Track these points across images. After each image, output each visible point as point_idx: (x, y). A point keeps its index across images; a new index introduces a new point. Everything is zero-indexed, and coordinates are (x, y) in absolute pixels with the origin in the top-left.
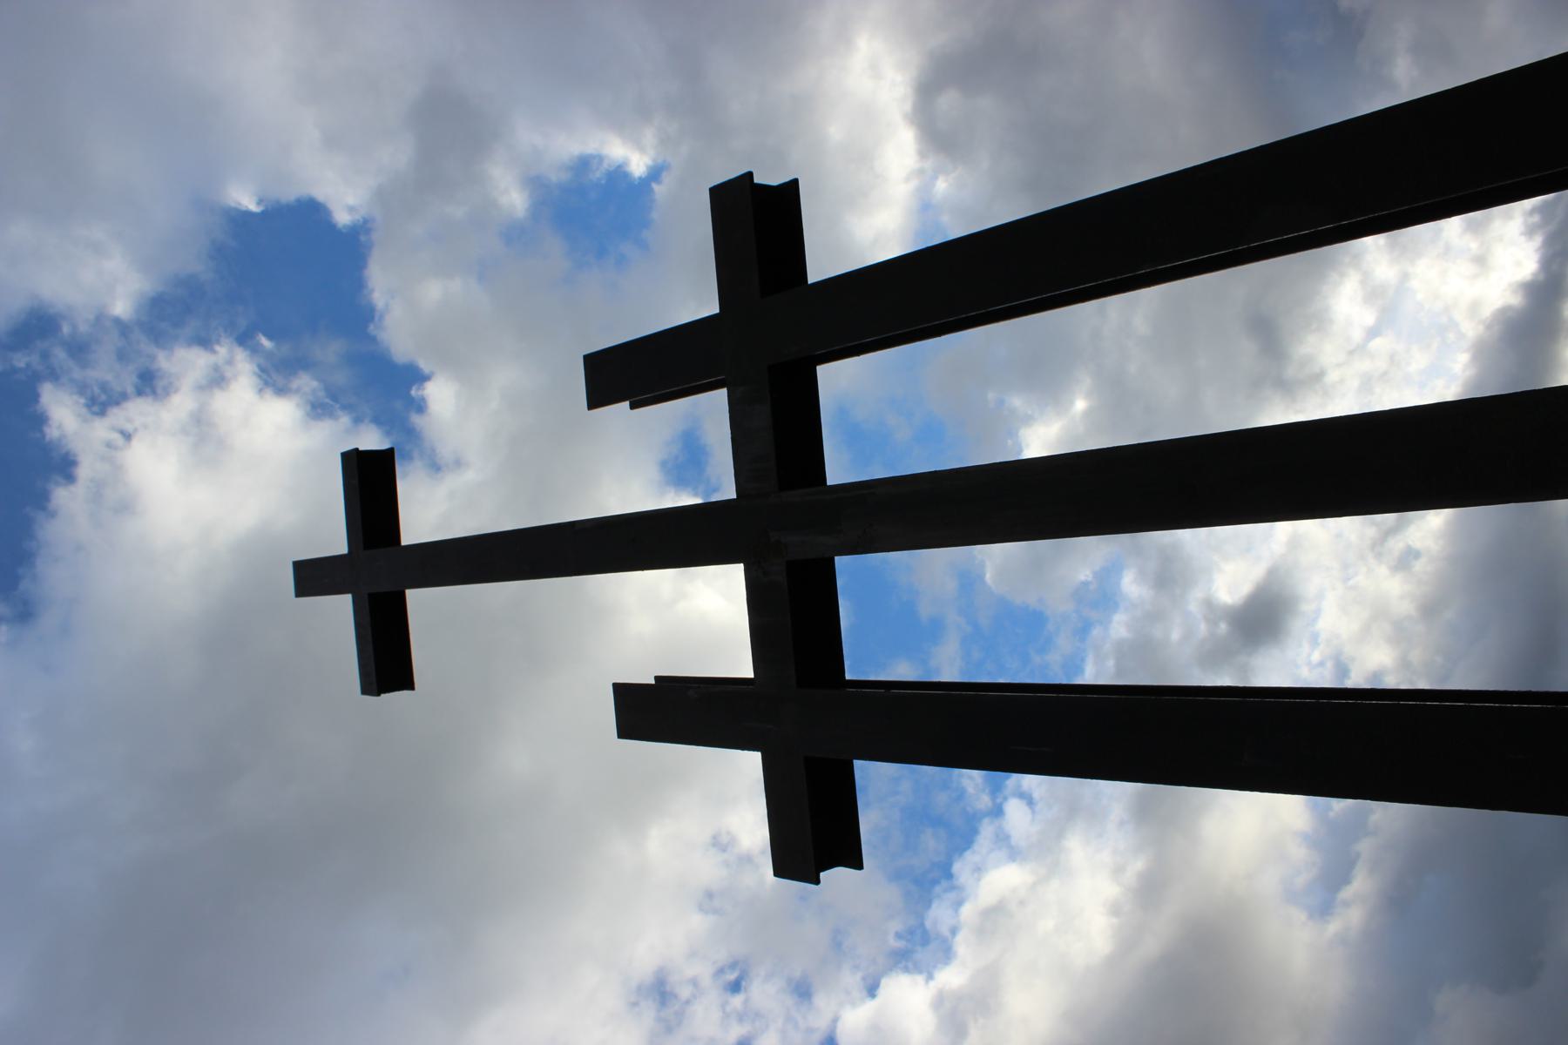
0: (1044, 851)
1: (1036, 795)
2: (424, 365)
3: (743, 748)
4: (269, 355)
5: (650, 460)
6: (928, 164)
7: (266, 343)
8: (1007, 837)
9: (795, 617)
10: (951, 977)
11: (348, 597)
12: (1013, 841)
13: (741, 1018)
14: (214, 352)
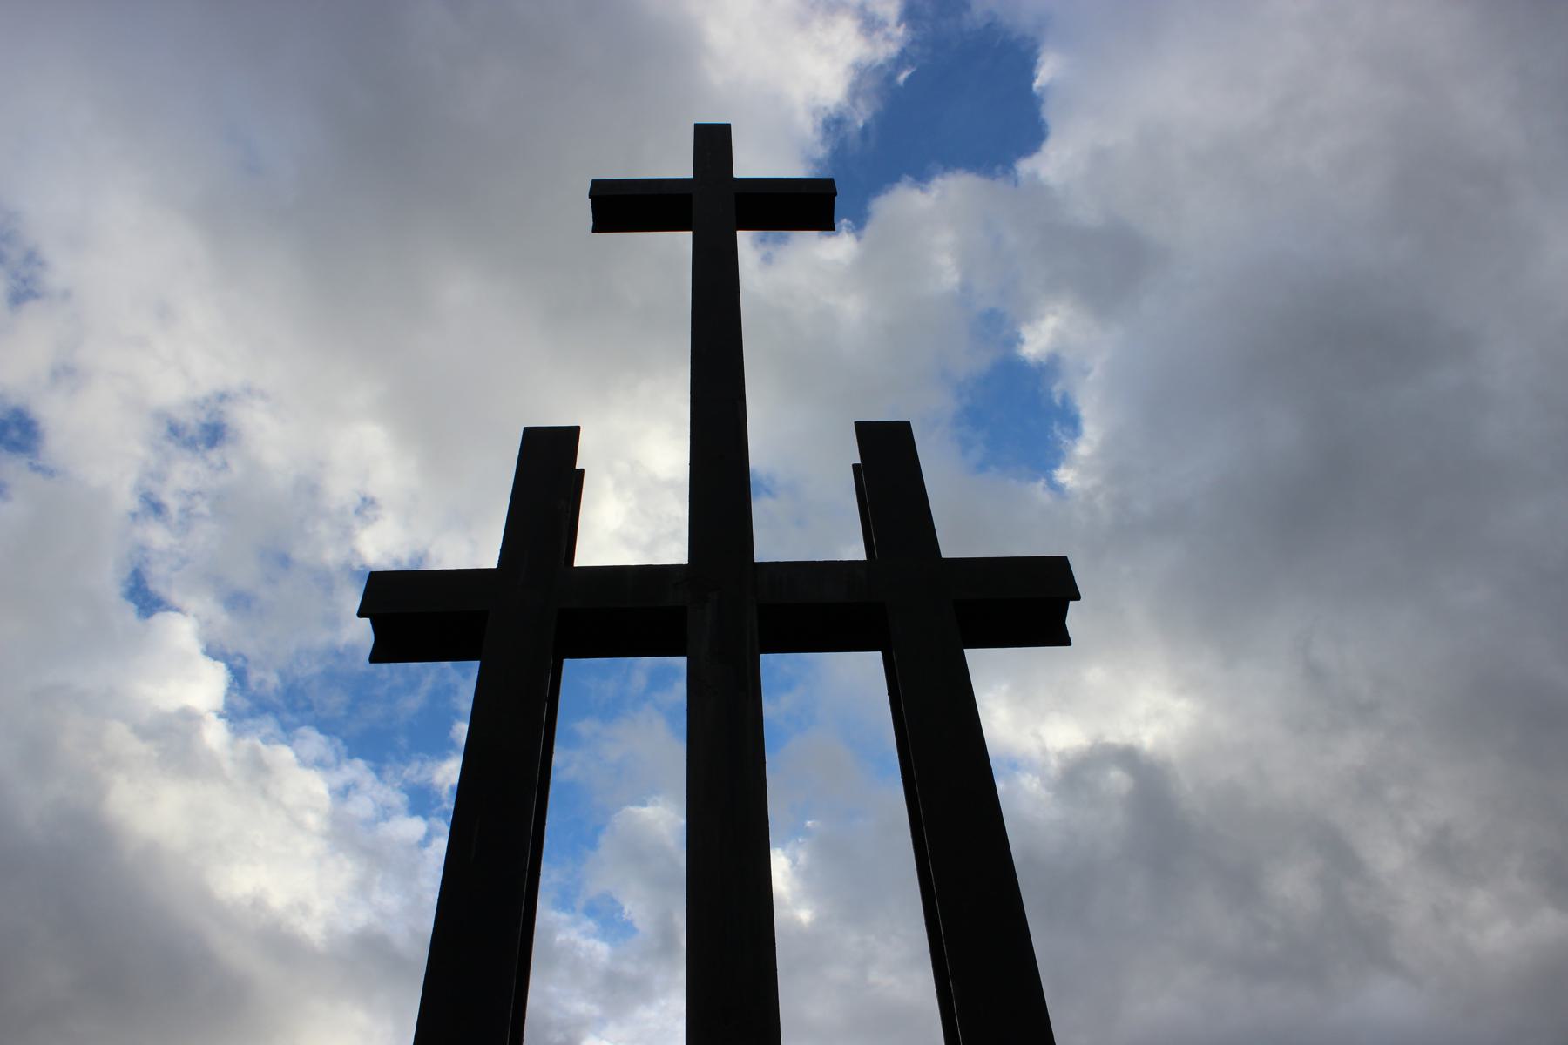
0: (345, 835)
1: (428, 851)
2: (870, 229)
3: (502, 550)
4: (890, 78)
5: (808, 516)
6: (1054, 762)
7: (902, 77)
8: (387, 819)
9: (630, 612)
10: (215, 734)
11: (689, 174)
12: (382, 824)
13: (186, 511)
14: (898, 25)
